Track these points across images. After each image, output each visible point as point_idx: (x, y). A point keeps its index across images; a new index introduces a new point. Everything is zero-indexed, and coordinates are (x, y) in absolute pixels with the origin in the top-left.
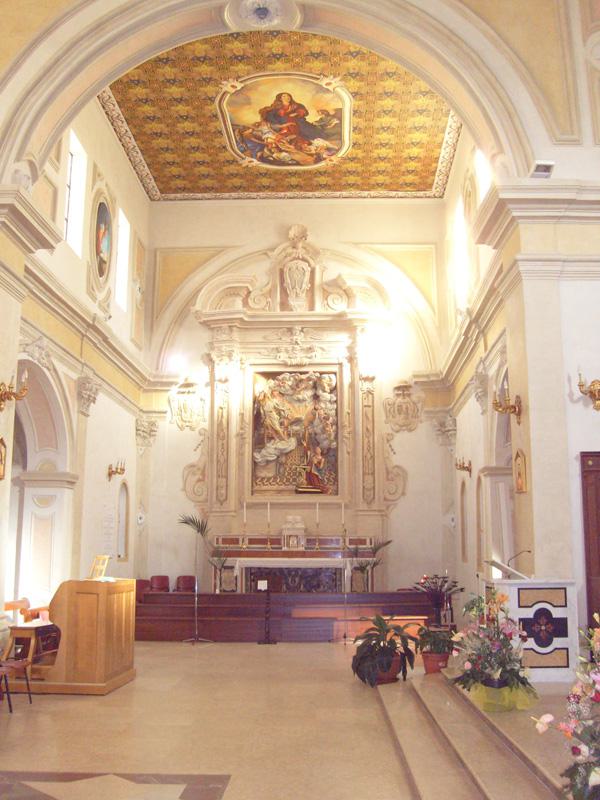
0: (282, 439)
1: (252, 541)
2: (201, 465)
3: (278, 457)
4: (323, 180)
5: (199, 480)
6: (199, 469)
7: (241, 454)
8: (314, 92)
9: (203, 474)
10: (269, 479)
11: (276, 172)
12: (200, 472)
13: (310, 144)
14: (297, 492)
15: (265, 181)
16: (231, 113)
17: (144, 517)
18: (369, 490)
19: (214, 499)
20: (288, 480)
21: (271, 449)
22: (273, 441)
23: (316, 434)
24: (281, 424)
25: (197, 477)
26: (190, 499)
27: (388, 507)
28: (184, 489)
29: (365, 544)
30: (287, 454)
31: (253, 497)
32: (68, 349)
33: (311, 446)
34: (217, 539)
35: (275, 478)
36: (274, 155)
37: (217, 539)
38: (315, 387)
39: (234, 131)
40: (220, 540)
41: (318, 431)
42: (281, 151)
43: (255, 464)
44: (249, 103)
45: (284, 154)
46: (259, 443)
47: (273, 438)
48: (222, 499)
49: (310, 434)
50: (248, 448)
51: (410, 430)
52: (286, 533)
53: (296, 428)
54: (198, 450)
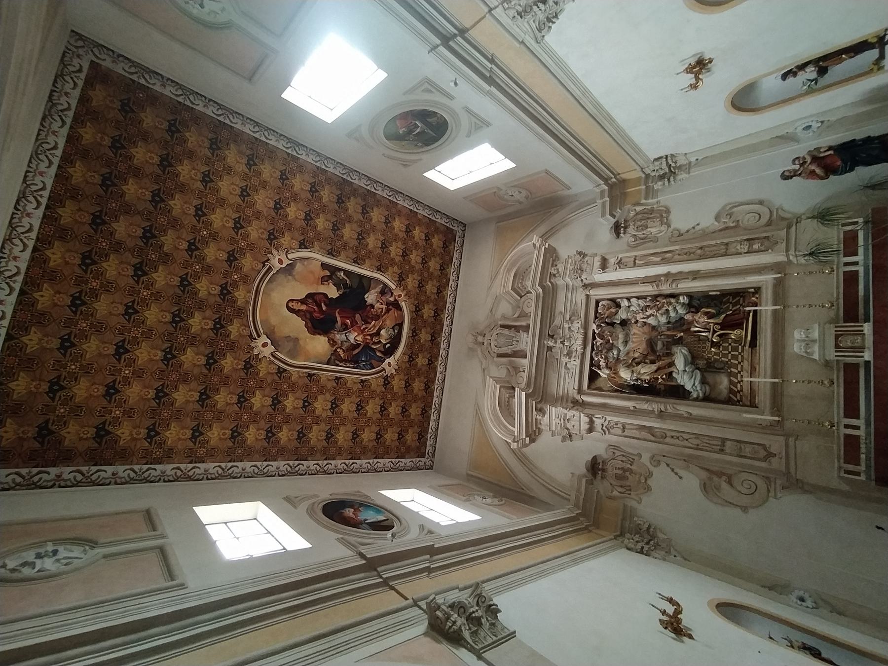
0: (672, 364)
1: (851, 410)
2: (704, 475)
3: (698, 369)
4: (428, 312)
5: (730, 483)
6: (710, 479)
7: (690, 418)
8: (290, 277)
9: (720, 474)
10: (731, 382)
11: (409, 346)
12: (715, 479)
13: (372, 306)
14: (753, 344)
15: (421, 361)
16: (309, 360)
17: (801, 593)
18: (750, 246)
19: (763, 464)
20: (735, 357)
21: (686, 379)
22: (674, 375)
23: (669, 323)
24: (653, 362)
25: (724, 486)
26: (766, 501)
27: (783, 219)
28: (745, 509)
29: (855, 237)
30: (693, 358)
31: (761, 406)
32: (797, 456)
33: (685, 327)
34: (848, 472)
35: (730, 374)
36: (384, 342)
37: (848, 472)
38: (612, 324)
39: (337, 365)
40: (851, 467)
41: (663, 319)
42: (378, 333)
43: (707, 399)
44: (296, 340)
45: (383, 332)
46: (678, 393)
47: (671, 373)
48: (763, 453)
49: (669, 329)
50: (683, 408)
51: (668, 211)
52: (831, 354)
53: (659, 346)
54: (681, 472)
